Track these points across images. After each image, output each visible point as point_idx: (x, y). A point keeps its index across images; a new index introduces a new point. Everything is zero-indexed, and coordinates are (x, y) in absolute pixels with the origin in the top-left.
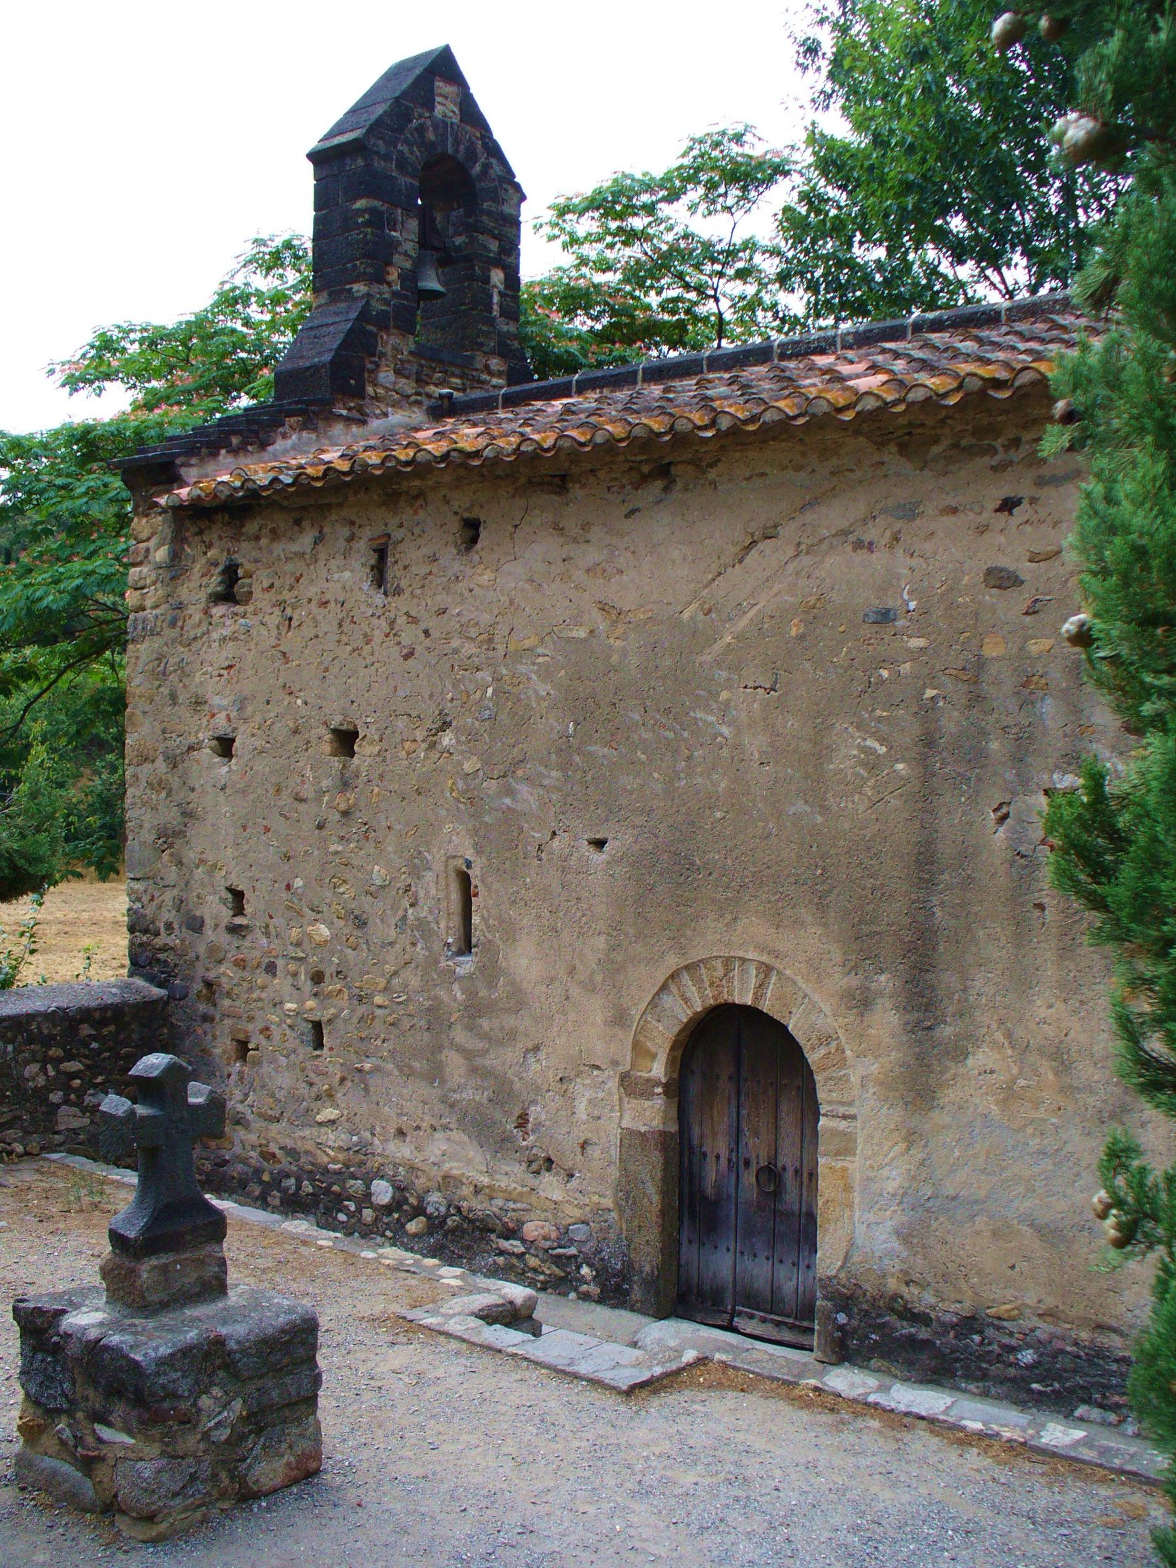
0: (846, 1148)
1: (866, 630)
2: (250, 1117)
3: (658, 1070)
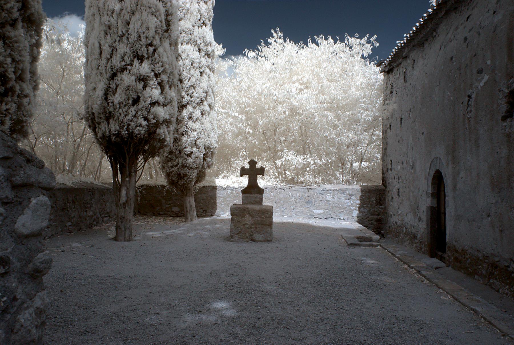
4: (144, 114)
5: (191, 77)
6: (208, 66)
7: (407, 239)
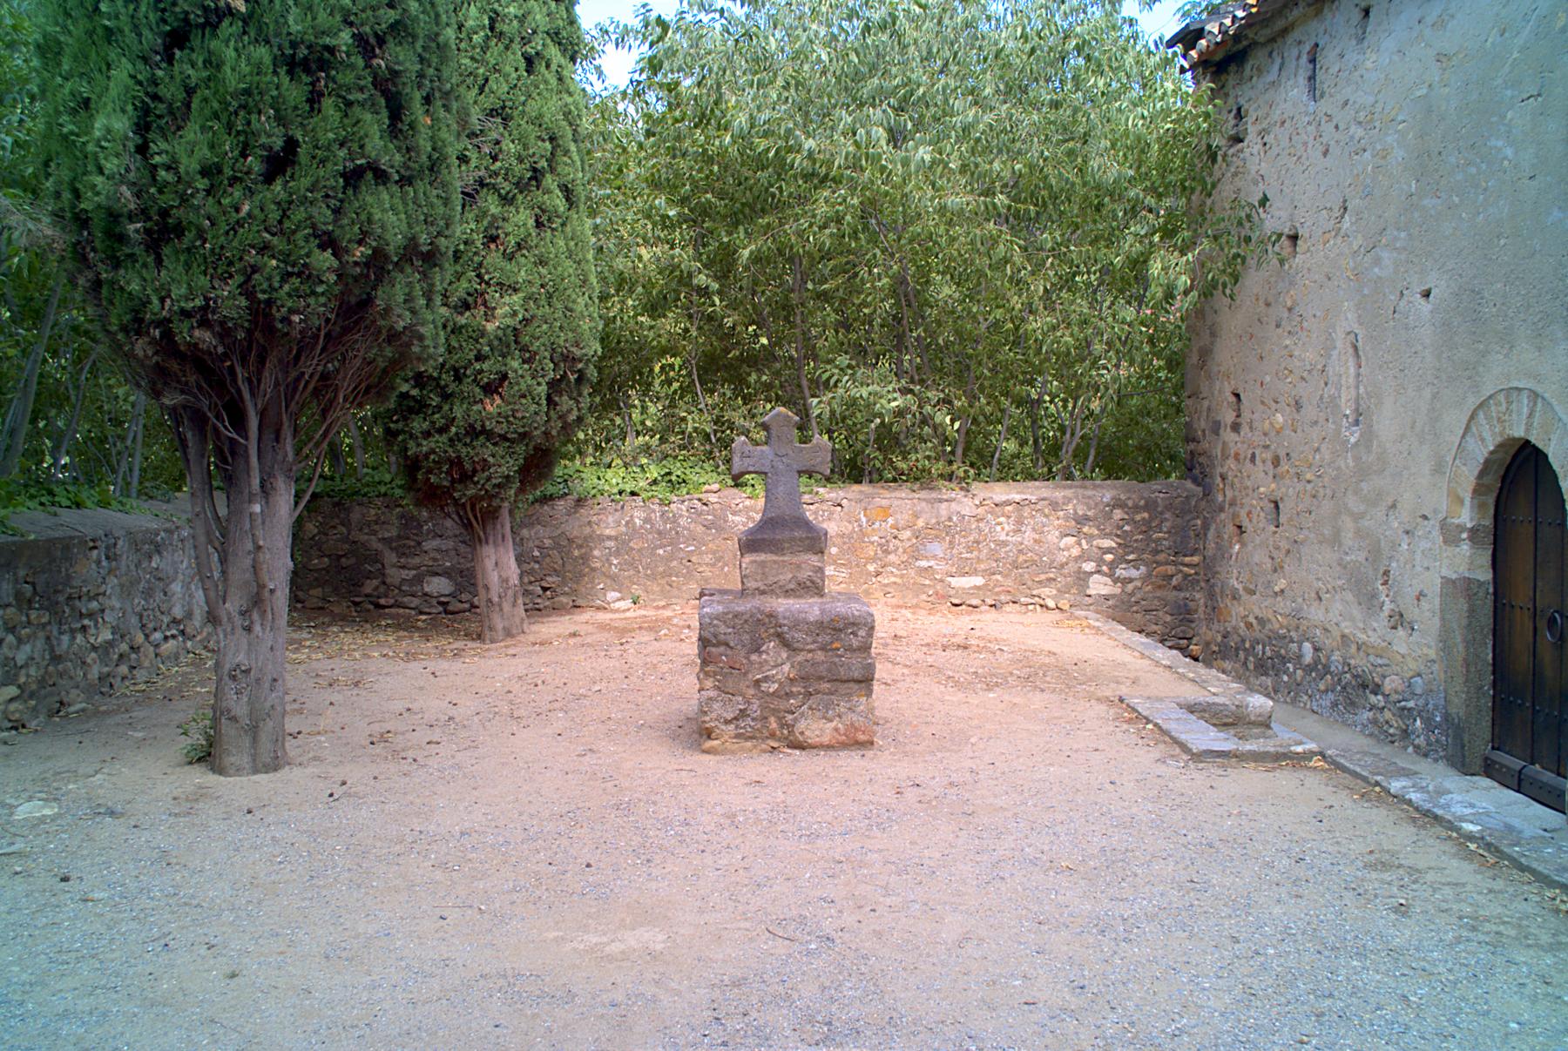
2: (1241, 592)
3: (1465, 517)
4: (319, 219)
5: (492, 78)
6: (555, 35)
7: (1322, 687)
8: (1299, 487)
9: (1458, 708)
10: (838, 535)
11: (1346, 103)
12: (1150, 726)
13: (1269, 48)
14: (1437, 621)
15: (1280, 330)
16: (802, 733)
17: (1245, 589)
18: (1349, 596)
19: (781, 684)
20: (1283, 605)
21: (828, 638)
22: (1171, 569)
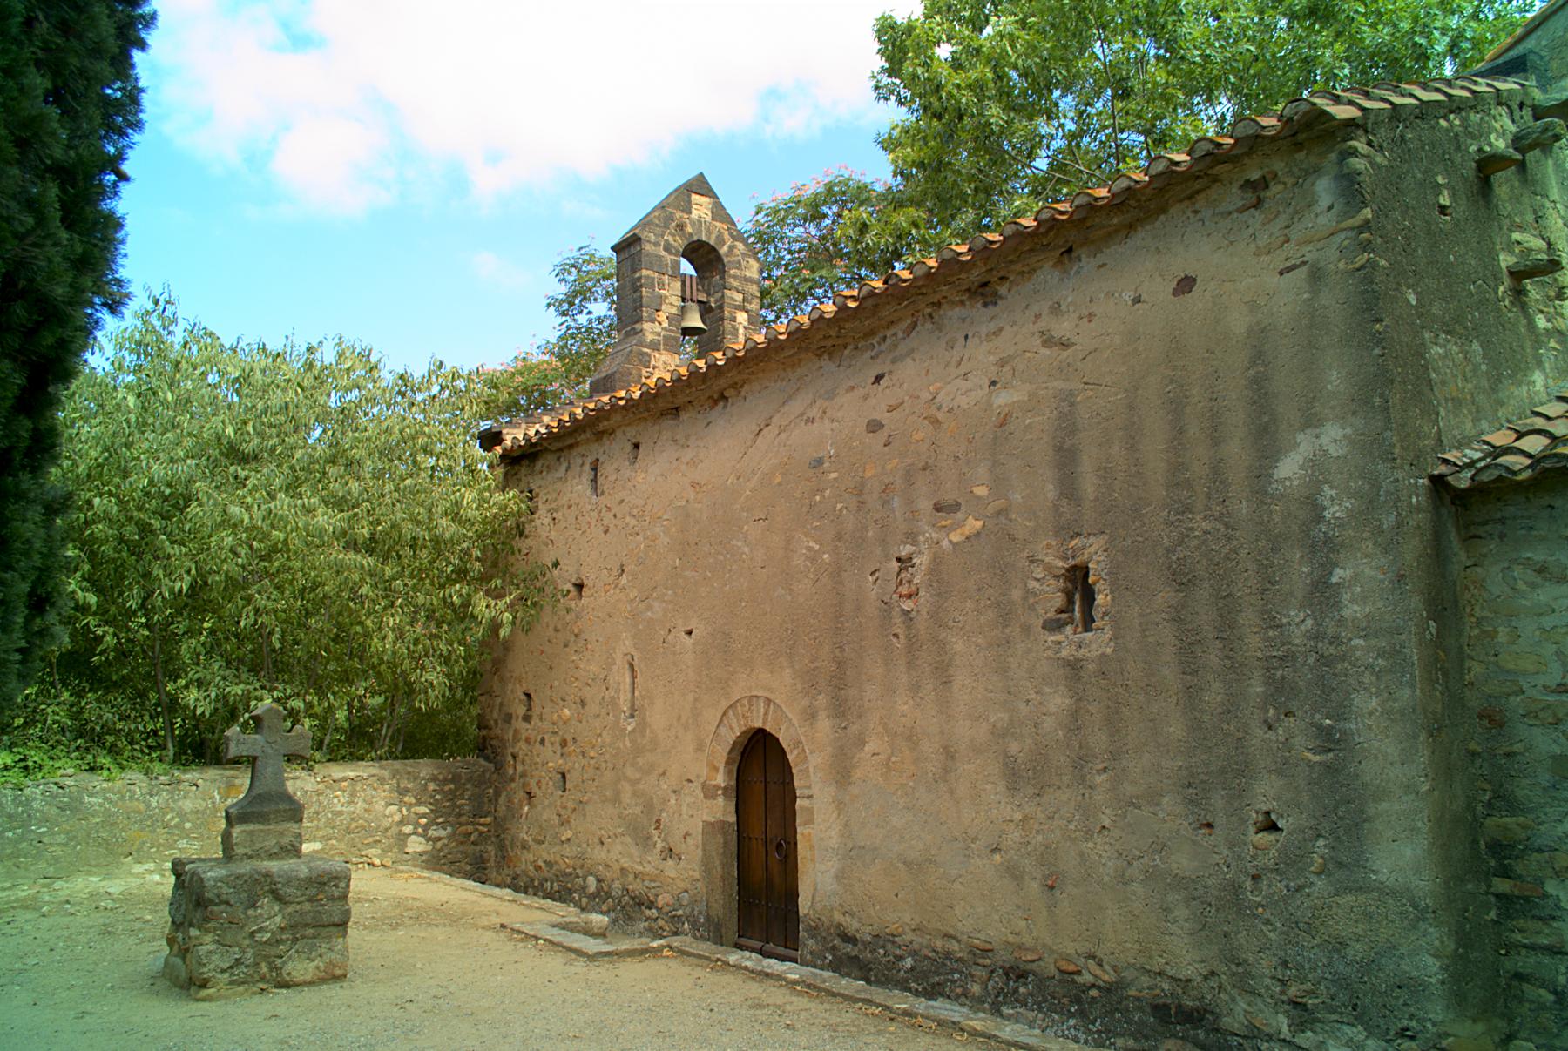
0: (810, 821)
1: (810, 473)
2: (530, 842)
3: (720, 779)
8: (584, 762)
9: (717, 910)
10: (192, 812)
11: (622, 501)
12: (541, 942)
13: (558, 454)
14: (700, 852)
15: (567, 649)
16: (289, 974)
17: (534, 840)
18: (628, 839)
19: (273, 933)
20: (568, 850)
21: (314, 891)
22: (470, 828)
